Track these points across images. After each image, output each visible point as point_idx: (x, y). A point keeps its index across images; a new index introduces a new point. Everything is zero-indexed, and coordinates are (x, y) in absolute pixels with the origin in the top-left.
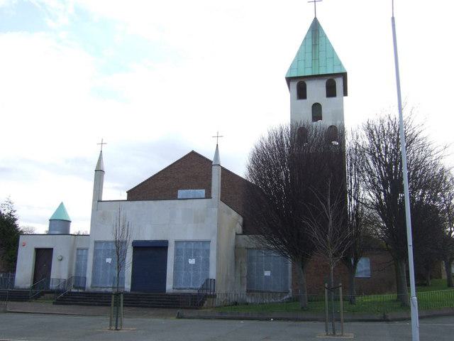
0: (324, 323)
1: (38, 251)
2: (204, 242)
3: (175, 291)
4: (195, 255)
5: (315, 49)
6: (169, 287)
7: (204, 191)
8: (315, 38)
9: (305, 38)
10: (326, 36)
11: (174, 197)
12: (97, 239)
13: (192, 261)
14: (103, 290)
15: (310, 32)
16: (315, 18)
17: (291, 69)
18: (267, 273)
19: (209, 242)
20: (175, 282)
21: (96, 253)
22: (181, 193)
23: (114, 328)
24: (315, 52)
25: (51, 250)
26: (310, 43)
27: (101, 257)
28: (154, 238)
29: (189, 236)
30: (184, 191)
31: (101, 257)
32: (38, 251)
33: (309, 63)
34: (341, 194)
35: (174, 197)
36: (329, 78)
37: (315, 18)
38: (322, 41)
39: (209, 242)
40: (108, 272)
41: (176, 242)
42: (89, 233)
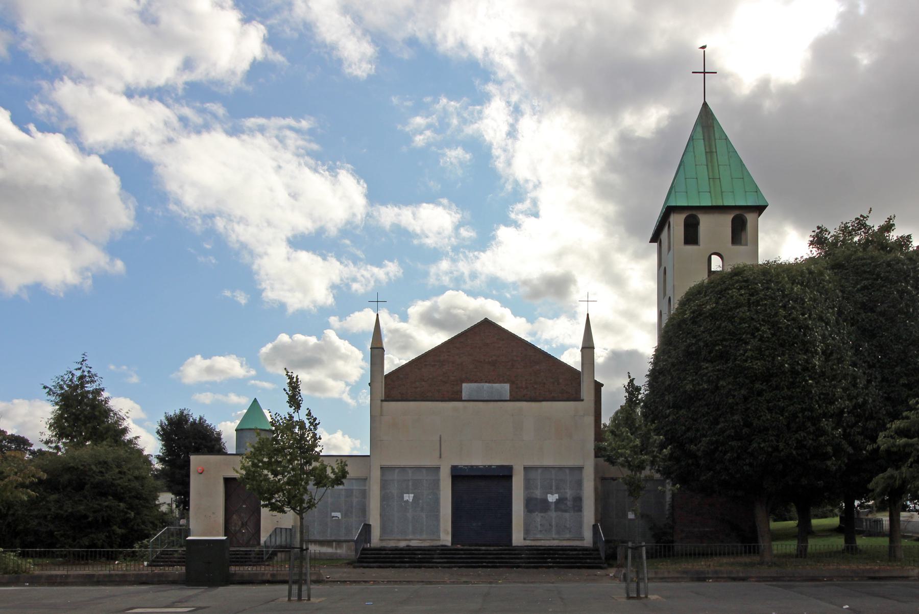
0: (624, 585)
2: (572, 469)
3: (528, 543)
6: (518, 538)
7: (507, 386)
8: (709, 139)
11: (456, 397)
13: (409, 497)
14: (402, 544)
16: (705, 105)
18: (631, 516)
19: (580, 469)
20: (527, 531)
21: (384, 485)
22: (467, 388)
23: (294, 598)
24: (713, 167)
30: (474, 385)
34: (262, 347)
36: (737, 212)
37: (705, 105)
38: (720, 146)
39: (580, 469)
40: (410, 515)
42: (369, 454)
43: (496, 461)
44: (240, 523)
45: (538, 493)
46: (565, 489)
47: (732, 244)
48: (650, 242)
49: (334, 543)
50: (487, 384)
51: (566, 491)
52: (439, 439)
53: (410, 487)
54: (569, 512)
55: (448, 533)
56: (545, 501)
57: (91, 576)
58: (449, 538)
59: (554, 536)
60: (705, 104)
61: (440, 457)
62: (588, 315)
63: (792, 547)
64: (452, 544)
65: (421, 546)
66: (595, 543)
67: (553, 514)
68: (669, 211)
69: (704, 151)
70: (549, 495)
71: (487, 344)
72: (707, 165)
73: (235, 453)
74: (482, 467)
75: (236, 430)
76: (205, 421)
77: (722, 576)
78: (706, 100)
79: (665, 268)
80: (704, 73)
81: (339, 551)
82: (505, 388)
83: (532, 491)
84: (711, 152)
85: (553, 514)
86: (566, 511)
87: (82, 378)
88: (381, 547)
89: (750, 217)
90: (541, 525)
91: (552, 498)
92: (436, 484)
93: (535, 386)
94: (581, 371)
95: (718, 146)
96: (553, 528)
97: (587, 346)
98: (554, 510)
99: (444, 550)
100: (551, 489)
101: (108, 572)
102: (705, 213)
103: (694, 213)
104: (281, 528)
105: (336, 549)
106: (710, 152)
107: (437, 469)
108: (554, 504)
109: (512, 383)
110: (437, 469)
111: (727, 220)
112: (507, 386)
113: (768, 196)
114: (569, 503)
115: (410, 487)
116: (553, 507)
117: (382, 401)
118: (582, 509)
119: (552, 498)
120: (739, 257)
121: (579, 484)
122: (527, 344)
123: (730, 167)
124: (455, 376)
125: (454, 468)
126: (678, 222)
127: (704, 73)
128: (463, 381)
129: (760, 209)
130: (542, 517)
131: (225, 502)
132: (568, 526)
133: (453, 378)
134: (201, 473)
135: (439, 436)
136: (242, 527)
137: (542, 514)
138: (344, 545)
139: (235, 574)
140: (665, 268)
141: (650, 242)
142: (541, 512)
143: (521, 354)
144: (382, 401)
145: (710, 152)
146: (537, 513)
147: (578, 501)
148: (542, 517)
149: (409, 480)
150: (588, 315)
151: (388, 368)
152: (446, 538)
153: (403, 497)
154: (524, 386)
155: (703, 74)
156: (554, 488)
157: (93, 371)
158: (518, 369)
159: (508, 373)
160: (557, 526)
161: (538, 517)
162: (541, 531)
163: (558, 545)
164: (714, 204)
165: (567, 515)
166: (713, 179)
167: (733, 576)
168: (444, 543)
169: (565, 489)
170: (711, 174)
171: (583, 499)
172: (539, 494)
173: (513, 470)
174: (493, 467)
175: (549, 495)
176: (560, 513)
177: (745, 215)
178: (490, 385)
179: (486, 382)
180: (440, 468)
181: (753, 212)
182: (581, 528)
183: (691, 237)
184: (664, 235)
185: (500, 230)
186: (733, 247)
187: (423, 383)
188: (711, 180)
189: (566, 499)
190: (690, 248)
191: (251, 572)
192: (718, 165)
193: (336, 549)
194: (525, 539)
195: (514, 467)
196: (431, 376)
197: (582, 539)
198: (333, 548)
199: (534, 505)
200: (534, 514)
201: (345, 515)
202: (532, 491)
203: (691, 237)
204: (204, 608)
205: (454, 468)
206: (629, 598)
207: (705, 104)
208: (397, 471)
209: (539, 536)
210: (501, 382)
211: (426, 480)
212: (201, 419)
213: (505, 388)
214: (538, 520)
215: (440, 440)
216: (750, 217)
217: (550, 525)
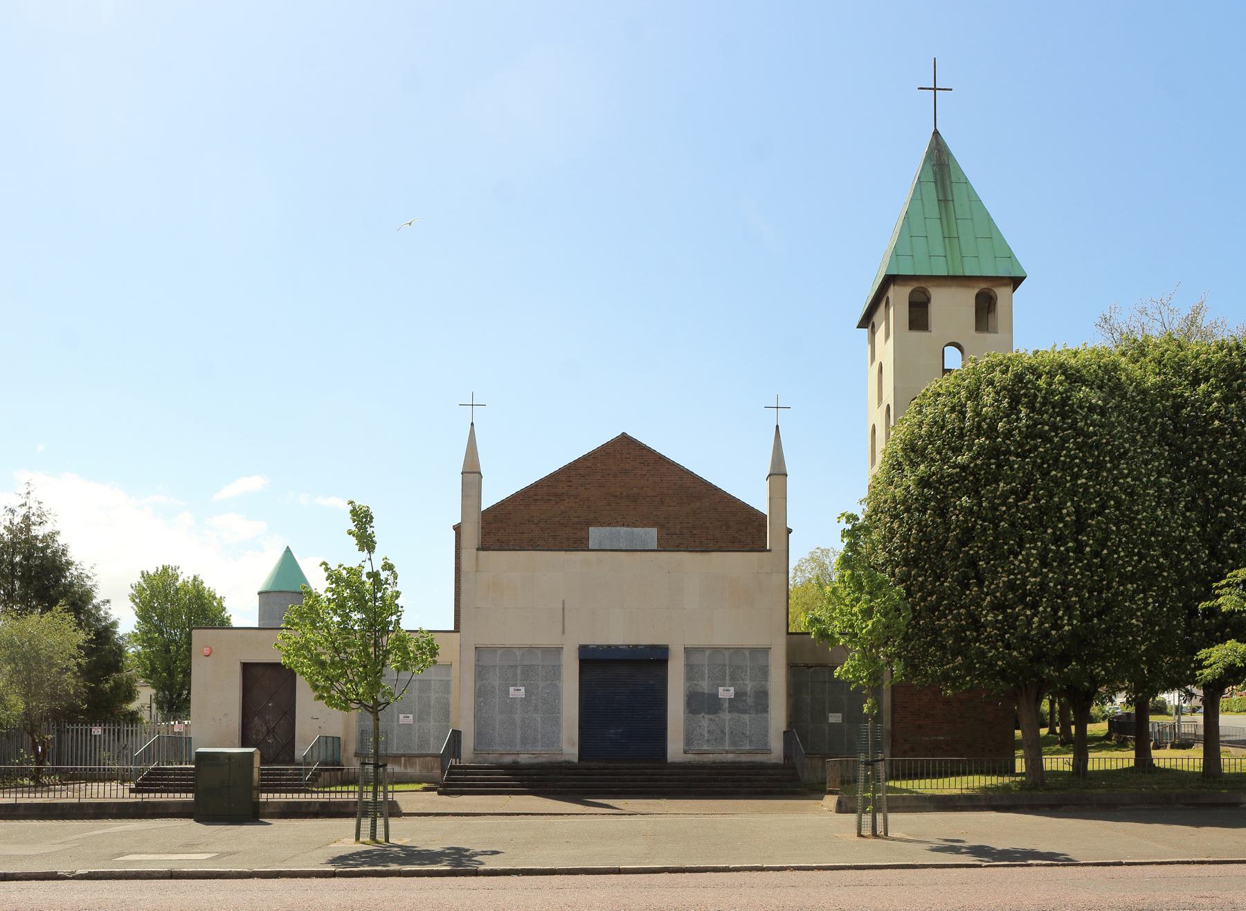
1: (249, 670)
2: (754, 651)
3: (690, 757)
4: (733, 678)
5: (946, 207)
6: (676, 749)
7: (653, 532)
9: (919, 181)
10: (967, 182)
12: (693, 642)
15: (929, 169)
17: (896, 254)
19: (766, 651)
20: (688, 741)
22: (596, 534)
25: (247, 668)
26: (931, 191)
27: (496, 683)
28: (632, 641)
29: (723, 636)
30: (605, 531)
31: (496, 683)
32: (249, 670)
33: (938, 247)
35: (579, 544)
36: (983, 285)
38: (957, 193)
39: (766, 651)
40: (518, 717)
41: (688, 651)
43: (645, 637)
44: (264, 729)
45: (705, 686)
46: (743, 681)
47: (976, 330)
48: (858, 327)
49: (403, 759)
51: (745, 682)
52: (562, 607)
53: (519, 677)
54: (749, 713)
55: (573, 745)
56: (714, 696)
57: (15, 806)
58: (575, 750)
59: (727, 748)
60: (936, 133)
61: (563, 633)
62: (777, 427)
63: (1126, 762)
64: (580, 759)
66: (787, 756)
67: (726, 716)
68: (889, 280)
69: (936, 199)
72: (941, 219)
73: (257, 626)
74: (624, 647)
75: (258, 594)
76: (202, 583)
77: (980, 804)
79: (881, 364)
80: (935, 89)
81: (409, 770)
82: (650, 535)
83: (695, 682)
84: (946, 200)
85: (726, 716)
86: (745, 712)
87: (26, 518)
89: (1001, 293)
90: (709, 731)
91: (726, 693)
92: (555, 672)
93: (694, 532)
94: (766, 511)
95: (955, 193)
96: (727, 735)
97: (776, 472)
98: (727, 711)
100: (724, 679)
101: (76, 801)
102: (939, 286)
105: (405, 766)
106: (945, 200)
107: (559, 650)
108: (727, 702)
109: (661, 526)
110: (559, 650)
111: (966, 299)
112: (653, 532)
113: (1026, 262)
114: (750, 701)
116: (726, 705)
117: (478, 549)
118: (769, 709)
119: (726, 693)
120: (987, 350)
121: (764, 672)
122: (682, 470)
123: (927, 240)
124: (579, 517)
125: (583, 649)
126: (899, 296)
127: (935, 89)
128: (589, 524)
129: (1016, 281)
130: (711, 720)
131: (243, 698)
132: (748, 733)
133: (576, 520)
134: (208, 656)
135: (561, 601)
136: (268, 734)
137: (710, 716)
138: (418, 761)
139: (266, 803)
140: (881, 364)
141: (858, 327)
142: (709, 713)
143: (576, 512)
144: (478, 549)
145: (945, 200)
146: (703, 714)
147: (762, 696)
148: (711, 720)
149: (516, 666)
150: (777, 427)
151: (488, 501)
154: (678, 532)
155: (933, 91)
156: (727, 678)
157: (45, 507)
158: (670, 506)
159: (655, 513)
160: (732, 733)
161: (705, 721)
162: (708, 740)
163: (733, 760)
165: (746, 717)
166: (949, 237)
167: (994, 803)
168: (567, 758)
169: (743, 681)
170: (946, 230)
171: (769, 693)
172: (706, 687)
173: (669, 652)
174: (639, 647)
176: (736, 715)
177: (994, 289)
178: (629, 529)
179: (623, 525)
181: (1005, 285)
182: (767, 736)
183: (918, 317)
184: (878, 317)
185: (72, 555)
186: (977, 335)
188: (947, 240)
189: (746, 693)
190: (917, 335)
191: (291, 800)
192: (956, 219)
193: (405, 766)
194: (685, 752)
195: (670, 647)
196: (543, 517)
197: (769, 752)
198: (401, 766)
199: (699, 703)
200: (698, 716)
201: (420, 718)
202: (695, 682)
203: (918, 317)
204: (235, 853)
205: (583, 649)
206: (860, 835)
207: (936, 133)
209: (705, 747)
210: (644, 526)
211: (543, 666)
212: (195, 579)
213: (650, 535)
214: (705, 723)
215: (563, 608)
216: (1001, 293)
217: (722, 732)
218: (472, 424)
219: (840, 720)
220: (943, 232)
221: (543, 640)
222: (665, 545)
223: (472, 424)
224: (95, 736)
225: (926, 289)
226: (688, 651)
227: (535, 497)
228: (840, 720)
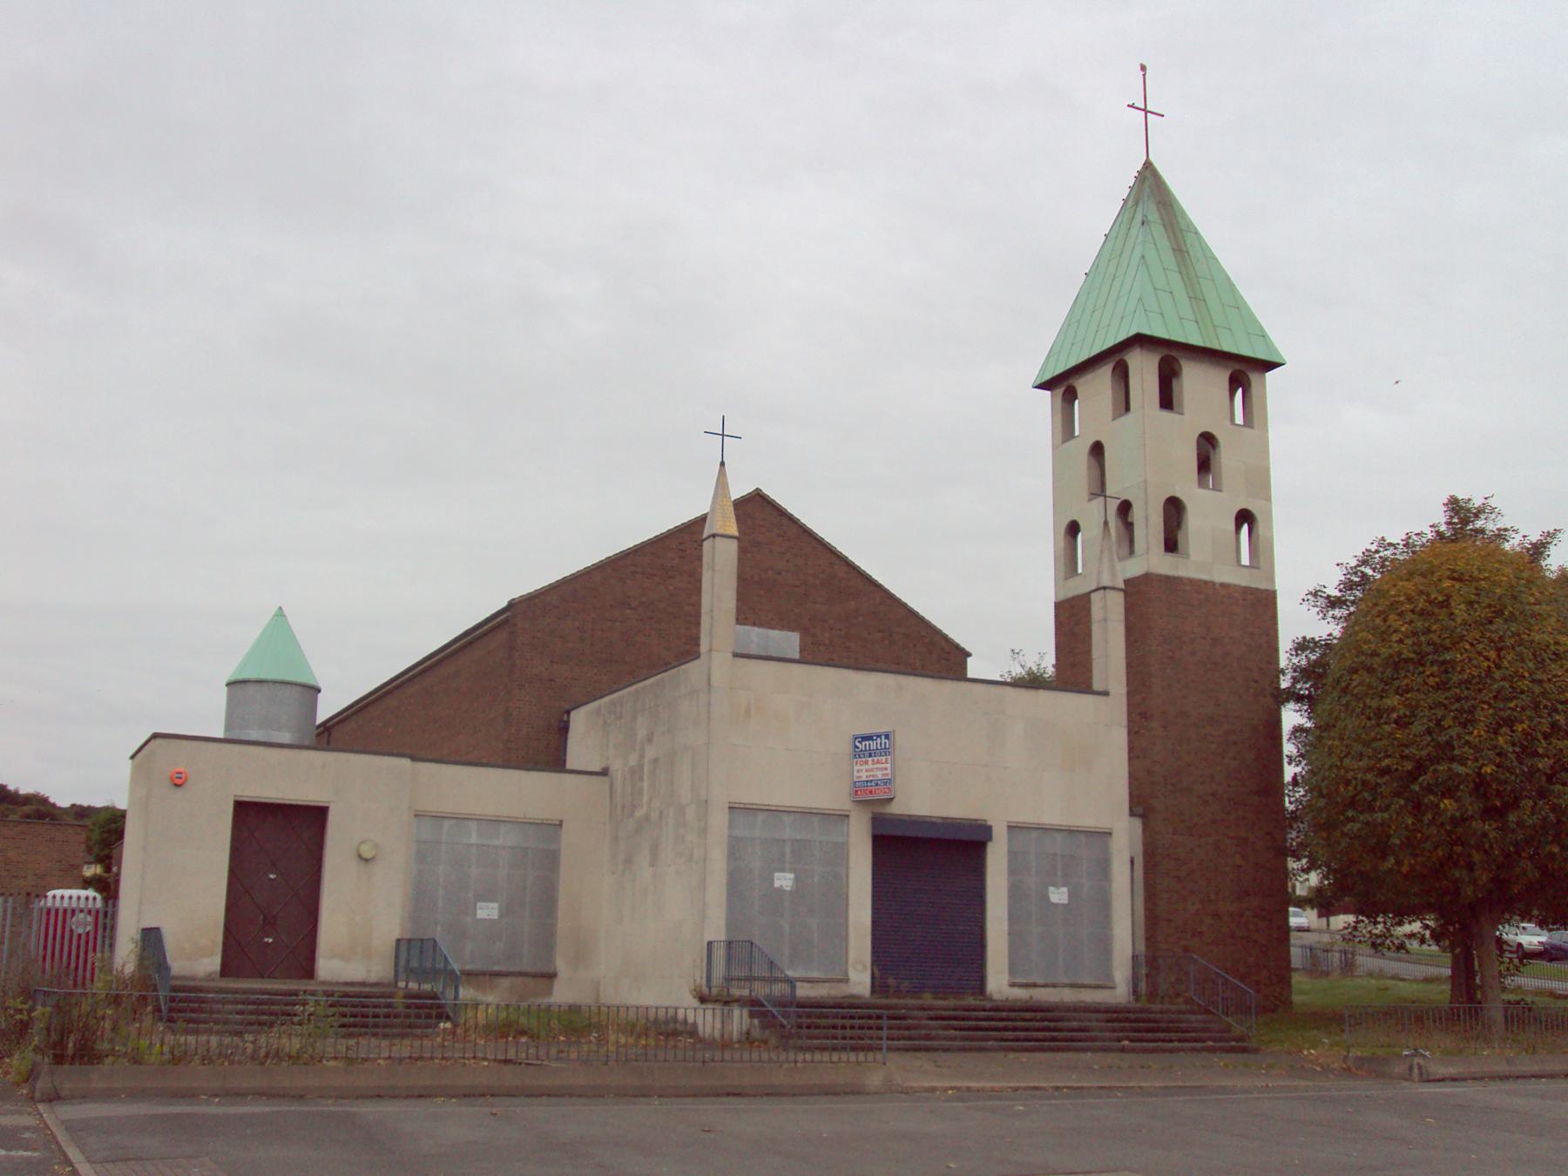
2: (1090, 833)
3: (1021, 994)
6: (998, 982)
16: (1148, 165)
36: (1237, 366)
41: (1011, 828)
50: (756, 629)
53: (788, 856)
55: (865, 967)
58: (866, 978)
65: (808, 998)
70: (1051, 889)
71: (758, 543)
72: (1180, 273)
78: (1150, 157)
82: (790, 641)
88: (1081, 1002)
99: (1113, 1015)
103: (1174, 353)
104: (422, 940)
109: (805, 632)
115: (788, 856)
129: (1270, 366)
138: (505, 983)
149: (784, 841)
152: (860, 981)
153: (1070, 897)
154: (827, 642)
164: (1208, 345)
175: (1051, 889)
179: (754, 624)
180: (1110, 834)
187: (628, 611)
208: (761, 817)
210: (782, 628)
218: (722, 464)
219: (494, 915)
220: (1188, 293)
221: (1088, 820)
222: (813, 654)
223: (722, 464)
224: (80, 935)
225: (1177, 361)
226: (1011, 828)
227: (633, 568)
228: (494, 915)
